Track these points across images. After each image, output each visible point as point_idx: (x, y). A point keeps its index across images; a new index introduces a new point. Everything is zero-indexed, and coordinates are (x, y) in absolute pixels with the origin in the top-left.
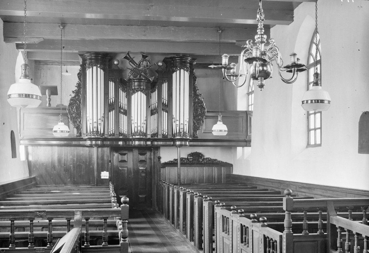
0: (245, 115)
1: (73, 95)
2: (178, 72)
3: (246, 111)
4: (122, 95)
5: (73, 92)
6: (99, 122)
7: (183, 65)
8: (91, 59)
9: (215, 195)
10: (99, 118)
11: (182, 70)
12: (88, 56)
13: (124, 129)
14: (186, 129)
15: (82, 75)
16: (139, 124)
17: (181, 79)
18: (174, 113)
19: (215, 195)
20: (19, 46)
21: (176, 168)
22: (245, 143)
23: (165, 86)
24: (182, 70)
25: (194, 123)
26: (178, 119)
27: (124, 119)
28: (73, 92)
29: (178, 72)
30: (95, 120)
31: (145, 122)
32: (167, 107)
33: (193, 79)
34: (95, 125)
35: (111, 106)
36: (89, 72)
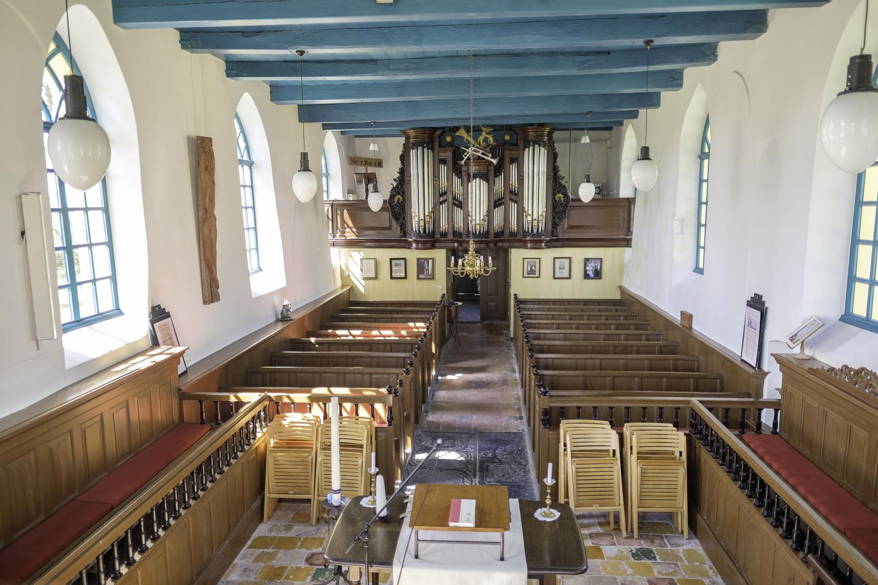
0: (626, 204)
1: (395, 184)
2: (531, 148)
3: (628, 199)
4: (456, 181)
5: (395, 180)
6: (427, 219)
7: (538, 141)
8: (415, 137)
9: (652, 68)
10: (427, 213)
11: (536, 146)
12: (412, 133)
13: (459, 224)
14: (542, 226)
15: (404, 158)
16: (478, 222)
17: (535, 165)
18: (525, 205)
19: (652, 68)
20: (325, 127)
21: (472, 525)
22: (625, 243)
23: (513, 170)
24: (536, 146)
25: (554, 218)
26: (530, 213)
27: (459, 214)
28: (395, 180)
29: (531, 148)
30: (422, 217)
31: (486, 218)
32: (516, 196)
33: (553, 157)
34: (422, 223)
35: (440, 196)
36: (413, 153)
